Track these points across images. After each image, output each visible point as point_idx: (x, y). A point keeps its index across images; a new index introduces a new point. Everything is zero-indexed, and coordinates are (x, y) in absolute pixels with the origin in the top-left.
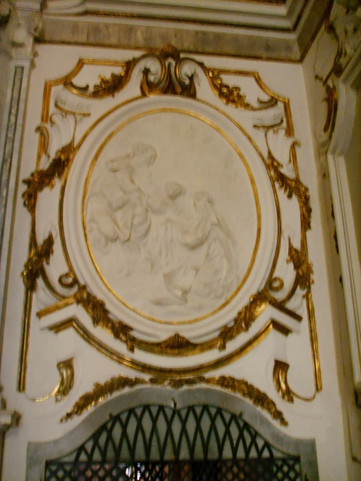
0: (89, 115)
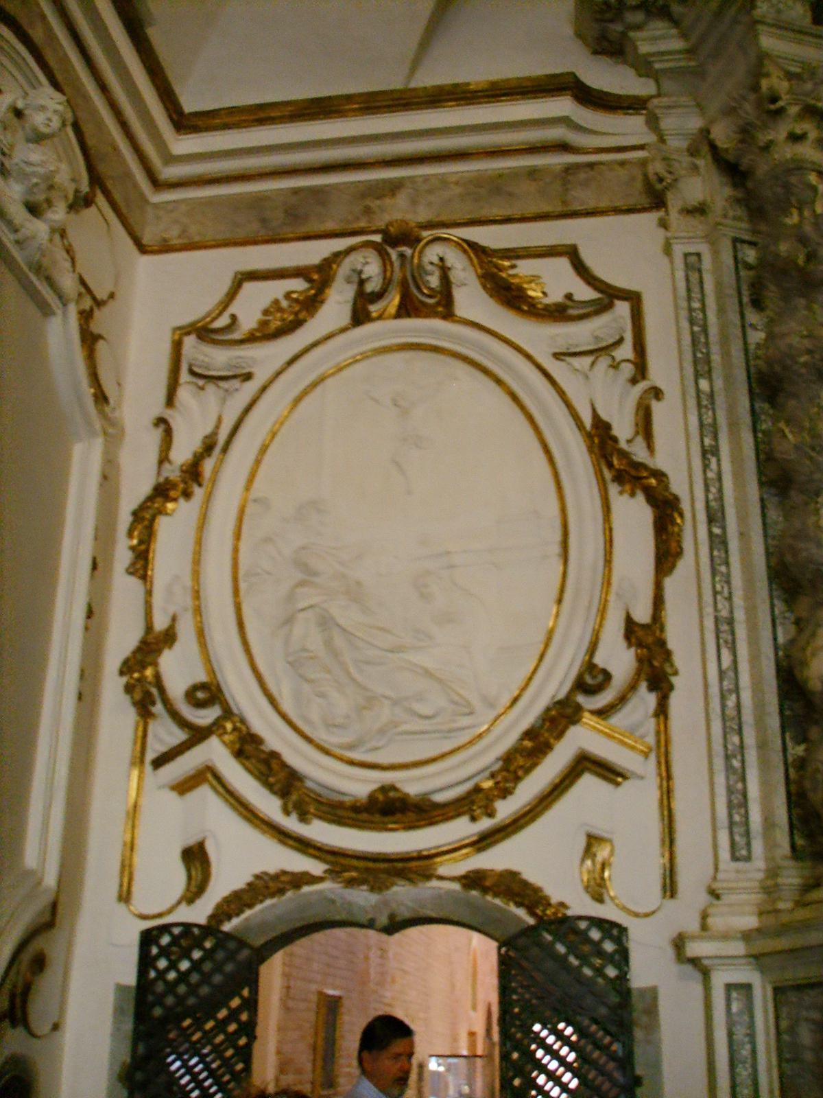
0: (248, 377)
